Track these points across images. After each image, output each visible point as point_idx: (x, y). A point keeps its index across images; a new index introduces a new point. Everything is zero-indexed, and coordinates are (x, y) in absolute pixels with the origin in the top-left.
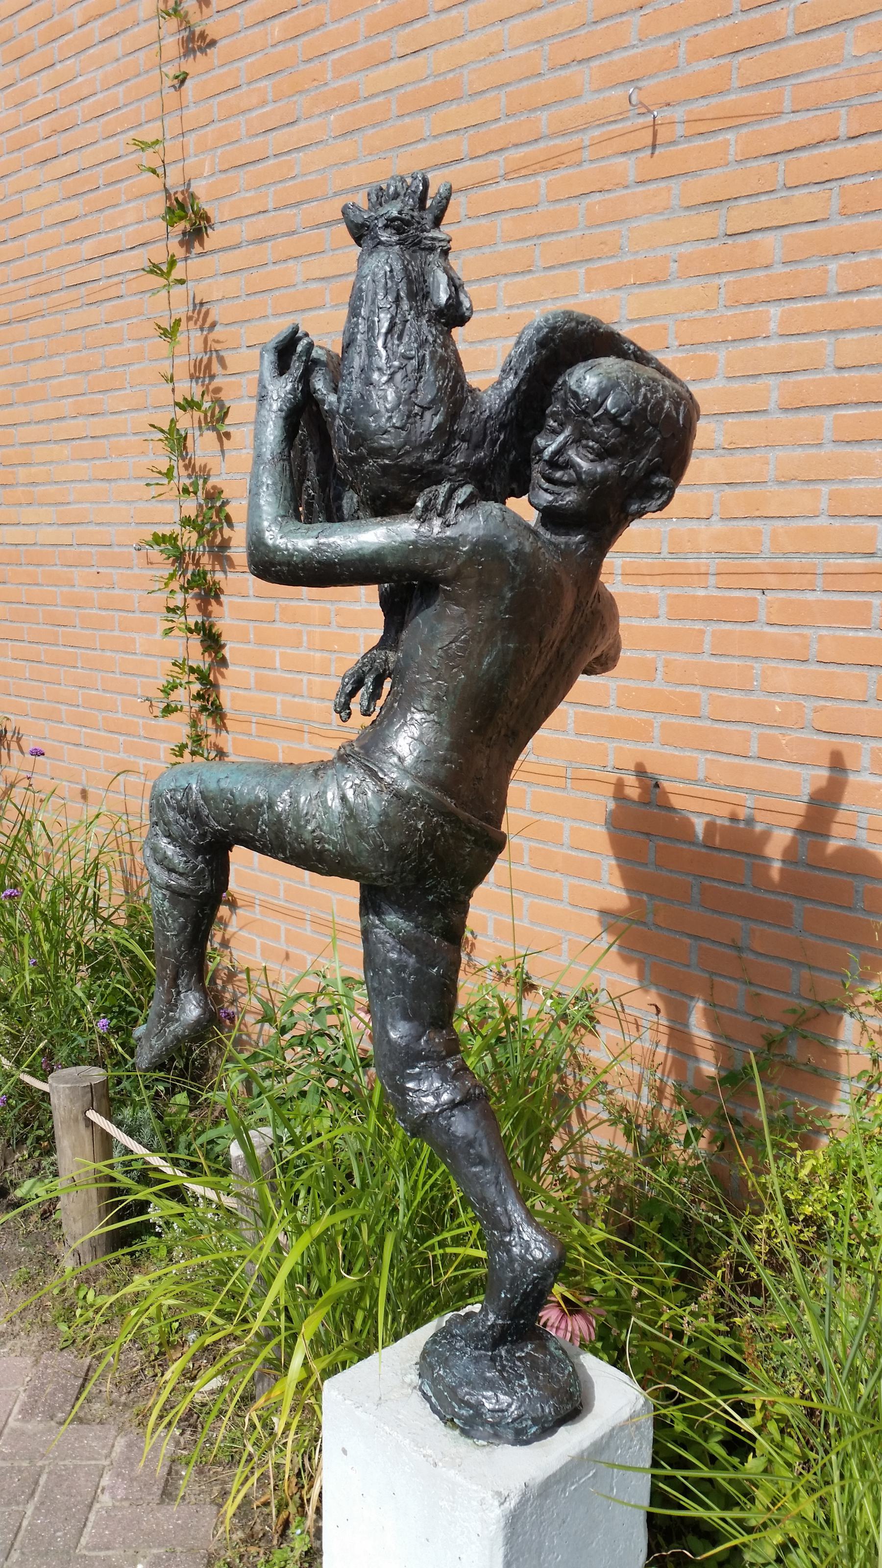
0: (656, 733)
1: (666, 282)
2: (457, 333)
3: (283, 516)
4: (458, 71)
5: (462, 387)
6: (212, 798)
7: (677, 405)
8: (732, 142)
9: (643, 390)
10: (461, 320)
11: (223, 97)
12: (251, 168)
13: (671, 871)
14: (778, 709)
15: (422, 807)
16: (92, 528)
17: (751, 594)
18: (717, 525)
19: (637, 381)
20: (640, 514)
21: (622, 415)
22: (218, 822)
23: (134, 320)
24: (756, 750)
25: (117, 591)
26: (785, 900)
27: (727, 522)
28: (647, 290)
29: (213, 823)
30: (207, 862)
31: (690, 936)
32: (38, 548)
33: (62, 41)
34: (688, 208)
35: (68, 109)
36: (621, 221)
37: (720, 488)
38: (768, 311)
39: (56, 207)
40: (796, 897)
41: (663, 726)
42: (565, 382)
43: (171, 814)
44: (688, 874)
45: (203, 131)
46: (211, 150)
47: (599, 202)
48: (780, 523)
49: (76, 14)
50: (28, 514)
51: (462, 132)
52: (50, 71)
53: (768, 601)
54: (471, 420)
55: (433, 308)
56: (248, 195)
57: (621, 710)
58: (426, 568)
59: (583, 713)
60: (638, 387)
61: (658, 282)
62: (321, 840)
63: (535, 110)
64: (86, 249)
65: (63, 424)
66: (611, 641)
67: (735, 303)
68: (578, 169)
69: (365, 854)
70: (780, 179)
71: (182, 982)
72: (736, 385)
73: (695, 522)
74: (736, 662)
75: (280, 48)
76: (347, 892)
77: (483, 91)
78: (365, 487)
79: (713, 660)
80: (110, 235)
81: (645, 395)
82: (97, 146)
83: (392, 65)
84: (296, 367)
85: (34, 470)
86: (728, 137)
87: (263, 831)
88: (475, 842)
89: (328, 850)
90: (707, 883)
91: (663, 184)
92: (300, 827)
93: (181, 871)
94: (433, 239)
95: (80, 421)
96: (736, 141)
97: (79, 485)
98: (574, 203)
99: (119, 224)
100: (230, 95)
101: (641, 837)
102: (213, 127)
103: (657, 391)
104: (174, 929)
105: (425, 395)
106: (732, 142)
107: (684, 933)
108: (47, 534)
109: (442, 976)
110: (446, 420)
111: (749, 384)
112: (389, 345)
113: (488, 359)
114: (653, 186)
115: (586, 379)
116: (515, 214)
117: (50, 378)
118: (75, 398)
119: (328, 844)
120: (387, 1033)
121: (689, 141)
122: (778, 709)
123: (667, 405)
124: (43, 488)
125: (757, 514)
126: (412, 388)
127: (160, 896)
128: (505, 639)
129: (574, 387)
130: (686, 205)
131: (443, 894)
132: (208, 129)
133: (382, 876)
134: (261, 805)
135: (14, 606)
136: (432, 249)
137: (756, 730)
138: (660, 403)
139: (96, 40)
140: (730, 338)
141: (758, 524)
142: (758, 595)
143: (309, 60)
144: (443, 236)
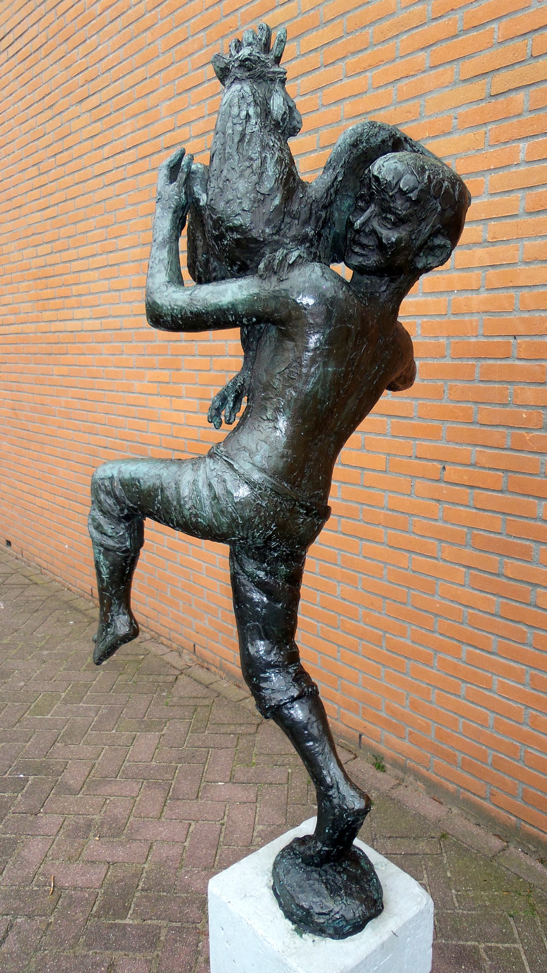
0: (443, 434)
1: (450, 133)
2: (292, 142)
3: (168, 282)
4: (316, 8)
5: (294, 179)
6: (127, 485)
7: (453, 185)
8: (496, 30)
9: (427, 172)
10: (294, 131)
11: (179, 47)
12: (195, 90)
13: (453, 524)
14: (524, 416)
15: (266, 490)
16: (111, 320)
17: (506, 339)
18: (484, 295)
19: (423, 168)
20: (427, 269)
21: (411, 191)
22: (131, 501)
23: (132, 193)
24: (509, 444)
25: (124, 356)
26: (528, 543)
27: (490, 292)
28: (438, 140)
29: (128, 502)
30: (127, 529)
31: (465, 566)
32: (83, 333)
33: (89, 25)
34: (465, 81)
35: (93, 67)
36: (421, 96)
37: (486, 269)
38: (518, 146)
39: (89, 128)
40: (535, 541)
41: (185, 388)
42: (369, 171)
43: (102, 496)
44: (464, 526)
45: (167, 70)
46: (172, 81)
47: (406, 84)
48: (525, 291)
49: (98, 8)
50: (78, 313)
51: (319, 50)
52: (84, 45)
53: (517, 343)
54: (300, 204)
55: (273, 123)
56: (193, 108)
57: (420, 420)
58: (267, 313)
59: (396, 422)
60: (423, 170)
61: (445, 134)
62: (196, 516)
63: (365, 27)
64: (106, 151)
65: (95, 259)
66: (407, 365)
67: (498, 143)
68: (393, 64)
69: (225, 525)
70: (528, 51)
71: (114, 608)
72: (497, 199)
73: (469, 292)
74: (497, 386)
75: (210, 10)
76: (225, 548)
77: (333, 19)
78: (226, 257)
79: (481, 385)
80: (118, 142)
81: (429, 176)
82: (110, 87)
83: (277, 11)
84: (182, 176)
85: (80, 287)
86: (493, 26)
87: (159, 508)
88: (306, 514)
89: (201, 522)
90: (476, 532)
91: (448, 66)
92: (180, 506)
93: (110, 534)
94: (274, 73)
95: (104, 256)
96: (499, 28)
97: (104, 295)
98: (390, 87)
99: (123, 134)
100: (182, 45)
101: (434, 503)
102: (173, 67)
103: (439, 174)
104: (107, 573)
105: (267, 185)
106: (496, 30)
107: (460, 565)
108: (89, 324)
109: (286, 609)
110: (281, 204)
111: (506, 197)
112: (241, 151)
113: (313, 160)
114: (441, 69)
115: (385, 166)
116: (352, 100)
117: (87, 232)
118: (101, 243)
119: (200, 518)
120: (248, 650)
121: (467, 34)
122: (524, 416)
123: (446, 183)
124: (86, 297)
125: (511, 284)
126: (257, 180)
127: (97, 551)
128: (325, 364)
129: (376, 173)
130: (463, 79)
131: (285, 551)
132: (170, 68)
133: (239, 540)
134: (156, 490)
135: (71, 367)
136: (272, 80)
137: (509, 431)
138: (440, 183)
139: (108, 21)
140: (492, 167)
141: (512, 292)
142: (512, 340)
143: (228, 15)
144: (282, 70)
